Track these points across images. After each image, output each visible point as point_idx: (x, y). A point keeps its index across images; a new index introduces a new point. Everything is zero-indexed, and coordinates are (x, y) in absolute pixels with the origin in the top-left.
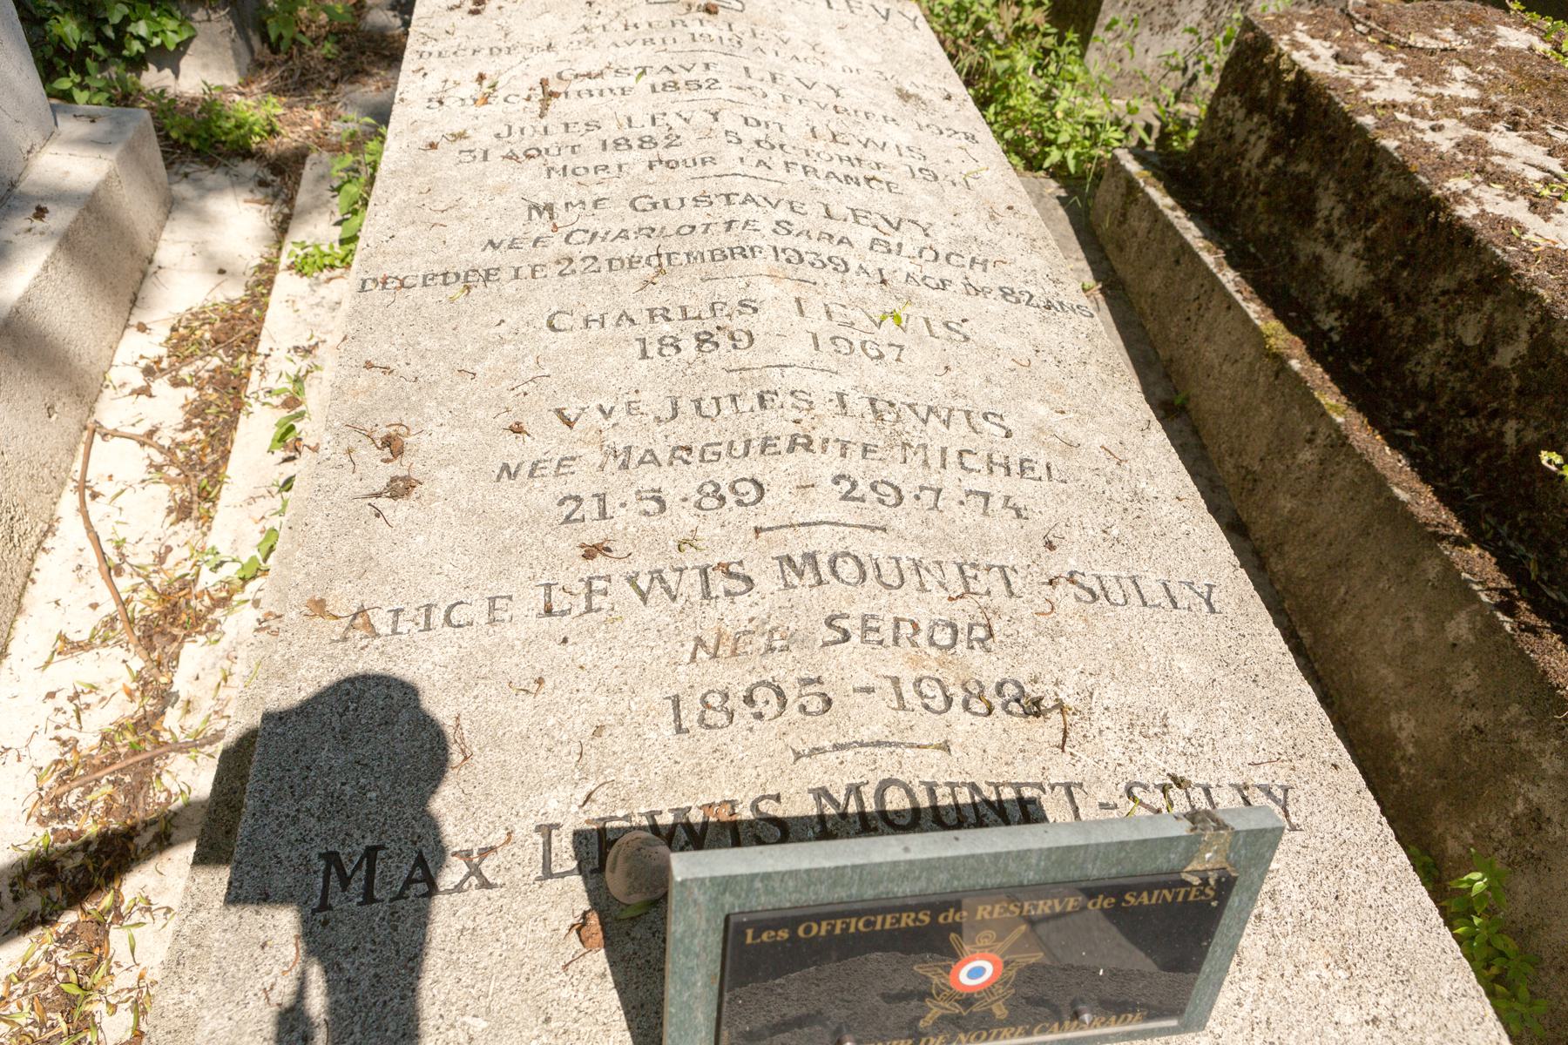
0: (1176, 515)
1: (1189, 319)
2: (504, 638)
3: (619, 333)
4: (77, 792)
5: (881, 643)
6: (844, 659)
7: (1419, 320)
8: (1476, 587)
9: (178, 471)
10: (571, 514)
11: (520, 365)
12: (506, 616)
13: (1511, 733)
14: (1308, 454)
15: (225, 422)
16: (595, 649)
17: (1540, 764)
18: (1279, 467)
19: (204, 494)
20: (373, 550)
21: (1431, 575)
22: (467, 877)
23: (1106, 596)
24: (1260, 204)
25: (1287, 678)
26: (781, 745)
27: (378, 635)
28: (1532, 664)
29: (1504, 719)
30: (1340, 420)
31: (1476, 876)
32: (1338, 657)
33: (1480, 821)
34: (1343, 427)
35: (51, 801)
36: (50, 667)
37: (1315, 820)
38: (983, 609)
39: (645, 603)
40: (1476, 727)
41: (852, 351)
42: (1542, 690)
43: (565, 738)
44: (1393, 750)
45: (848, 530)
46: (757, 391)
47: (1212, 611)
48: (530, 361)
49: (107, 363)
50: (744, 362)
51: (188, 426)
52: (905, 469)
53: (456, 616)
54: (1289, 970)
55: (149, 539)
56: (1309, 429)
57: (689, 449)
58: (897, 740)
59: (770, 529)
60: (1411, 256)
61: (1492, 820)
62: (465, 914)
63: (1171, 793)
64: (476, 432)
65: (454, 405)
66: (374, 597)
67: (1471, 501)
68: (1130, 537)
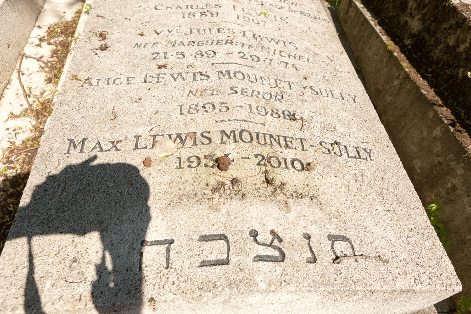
0: (347, 77)
1: (364, 43)
2: (131, 88)
3: (177, 11)
4: (14, 156)
5: (247, 95)
6: (235, 98)
7: (436, 39)
8: (443, 119)
9: (48, 69)
10: (155, 57)
11: (145, 18)
12: (132, 82)
13: (449, 163)
14: (397, 82)
15: (64, 56)
16: (158, 92)
17: (457, 172)
18: (388, 87)
19: (56, 76)
20: (93, 64)
21: (430, 116)
22: (112, 148)
23: (321, 94)
24: (390, 6)
25: (376, 122)
26: (212, 119)
27: (93, 85)
28: (458, 141)
29: (447, 159)
30: (407, 70)
31: (433, 205)
32: (400, 144)
33: (437, 191)
34: (408, 72)
35: (7, 158)
36: (8, 122)
37: (379, 159)
38: (281, 92)
39: (175, 81)
40: (439, 162)
41: (249, 21)
42: (462, 149)
43: (146, 114)
44: (414, 171)
45: (241, 66)
46: (218, 28)
47: (355, 102)
48: (148, 17)
49: (28, 36)
50: (215, 20)
51: (52, 57)
52: (262, 53)
53: (116, 82)
54: (364, 194)
55: (39, 88)
56: (398, 74)
57: (194, 42)
58: (248, 120)
59: (217, 64)
60: (436, 18)
61: (441, 190)
62: (110, 157)
63: (334, 146)
64: (129, 35)
65: (123, 27)
66: (92, 75)
67: (446, 95)
68: (332, 80)
